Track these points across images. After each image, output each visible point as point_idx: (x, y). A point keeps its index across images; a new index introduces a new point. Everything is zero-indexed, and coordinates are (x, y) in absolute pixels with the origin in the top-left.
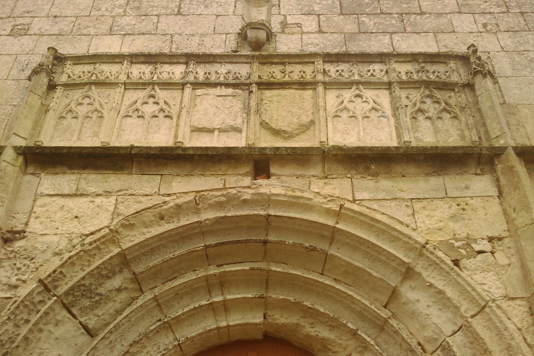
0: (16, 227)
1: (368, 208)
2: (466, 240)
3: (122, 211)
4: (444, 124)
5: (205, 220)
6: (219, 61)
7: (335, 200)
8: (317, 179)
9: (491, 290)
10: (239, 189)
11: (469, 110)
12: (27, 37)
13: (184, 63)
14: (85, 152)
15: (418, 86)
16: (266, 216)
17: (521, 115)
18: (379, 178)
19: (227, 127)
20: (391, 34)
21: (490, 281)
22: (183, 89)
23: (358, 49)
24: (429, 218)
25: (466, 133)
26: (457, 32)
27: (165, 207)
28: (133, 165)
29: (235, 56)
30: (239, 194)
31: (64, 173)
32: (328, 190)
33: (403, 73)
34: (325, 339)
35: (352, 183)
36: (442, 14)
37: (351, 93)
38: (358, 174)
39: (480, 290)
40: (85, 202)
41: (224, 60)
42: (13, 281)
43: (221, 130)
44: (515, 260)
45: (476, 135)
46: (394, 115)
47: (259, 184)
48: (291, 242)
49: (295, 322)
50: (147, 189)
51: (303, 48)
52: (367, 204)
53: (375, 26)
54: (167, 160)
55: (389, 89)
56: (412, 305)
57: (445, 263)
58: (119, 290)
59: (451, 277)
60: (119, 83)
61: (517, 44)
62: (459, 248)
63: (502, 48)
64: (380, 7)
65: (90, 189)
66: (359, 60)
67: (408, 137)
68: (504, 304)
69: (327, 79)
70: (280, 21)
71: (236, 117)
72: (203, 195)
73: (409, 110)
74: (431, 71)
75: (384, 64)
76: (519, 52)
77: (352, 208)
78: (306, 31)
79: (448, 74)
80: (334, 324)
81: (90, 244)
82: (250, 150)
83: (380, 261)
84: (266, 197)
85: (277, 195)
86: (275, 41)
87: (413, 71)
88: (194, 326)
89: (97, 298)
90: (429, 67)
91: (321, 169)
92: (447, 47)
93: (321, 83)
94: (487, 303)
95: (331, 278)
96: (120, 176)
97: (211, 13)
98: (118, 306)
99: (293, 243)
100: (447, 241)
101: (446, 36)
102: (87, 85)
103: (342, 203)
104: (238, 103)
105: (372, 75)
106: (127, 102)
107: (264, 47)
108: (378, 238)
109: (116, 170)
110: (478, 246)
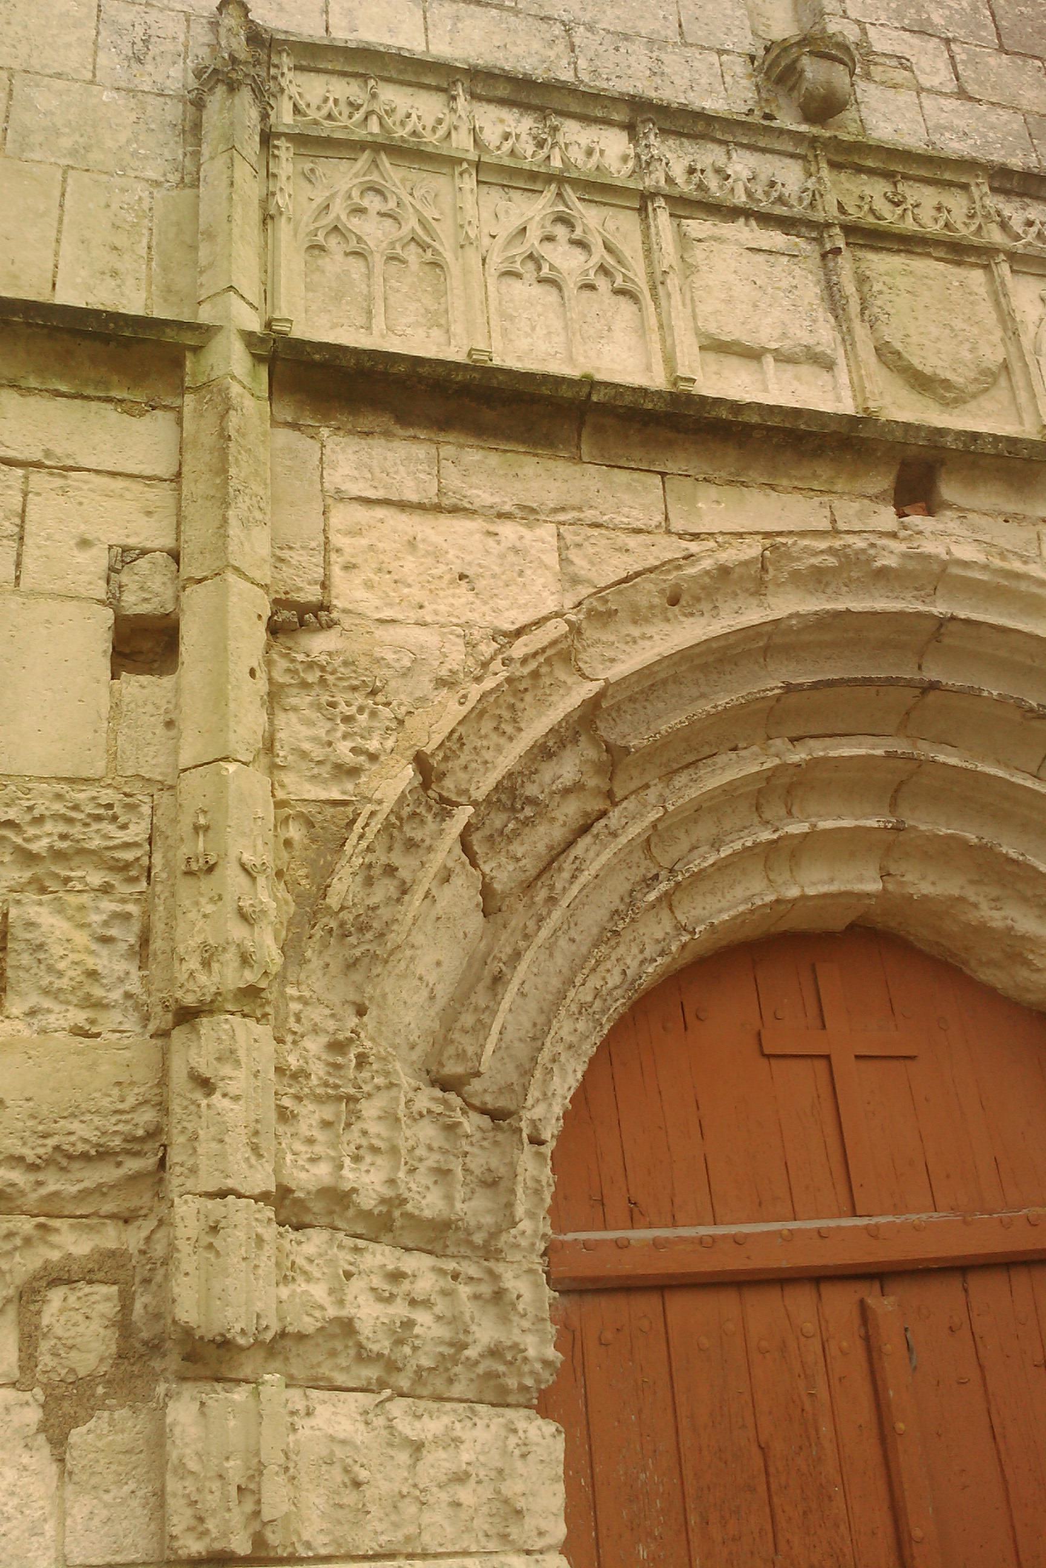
0: (299, 589)
3: (583, 572)
5: (791, 616)
6: (719, 135)
10: (873, 539)
14: (460, 378)
19: (797, 350)
22: (642, 210)
28: (580, 436)
30: (872, 552)
31: (387, 434)
34: (1030, 939)
40: (471, 534)
41: (735, 137)
42: (343, 749)
47: (916, 529)
48: (995, 693)
49: (956, 892)
54: (679, 432)
58: (567, 791)
60: (465, 160)
65: (479, 496)
71: (814, 321)
72: (785, 544)
81: (524, 661)
84: (935, 567)
85: (965, 564)
88: (719, 894)
96: (551, 464)
109: (535, 444)
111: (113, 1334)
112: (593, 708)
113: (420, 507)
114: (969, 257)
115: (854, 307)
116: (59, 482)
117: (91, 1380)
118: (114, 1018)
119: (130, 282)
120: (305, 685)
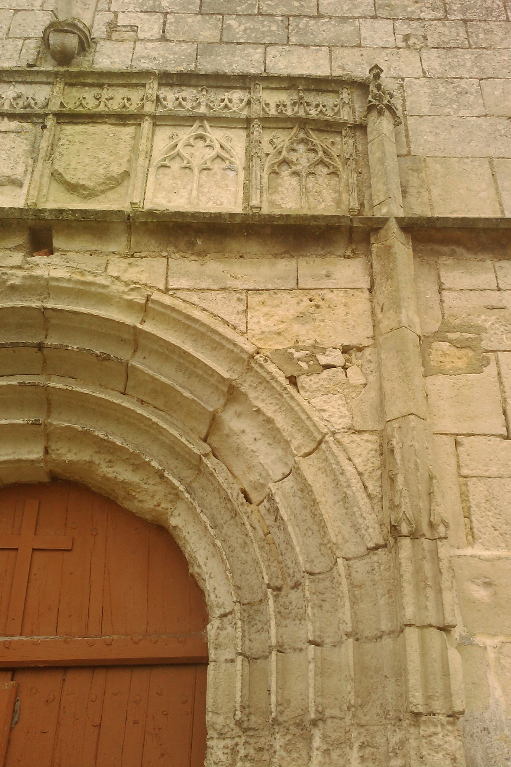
1: (184, 301)
2: (312, 349)
4: (316, 183)
7: (140, 288)
8: (118, 258)
9: (333, 420)
11: (354, 163)
15: (289, 125)
16: (40, 309)
17: (429, 173)
18: (207, 258)
20: (267, 45)
21: (333, 407)
22: (248, 128)
23: (213, 68)
24: (267, 317)
25: (344, 196)
26: (363, 47)
29: (30, 73)
30: (5, 277)
32: (132, 274)
33: (273, 106)
34: (126, 483)
35: (168, 264)
36: (348, 18)
37: (191, 133)
38: (178, 252)
39: (316, 419)
44: (375, 378)
45: (357, 200)
46: (248, 169)
47: (35, 263)
48: (75, 347)
49: (88, 458)
51: (133, 63)
53: (245, 34)
55: (248, 128)
56: (236, 437)
57: (277, 381)
59: (283, 400)
61: (447, 68)
62: (299, 360)
63: (424, 72)
64: (259, 4)
66: (212, 83)
67: (259, 200)
68: (346, 439)
69: (160, 110)
70: (107, 21)
71: (16, 163)
73: (268, 162)
74: (314, 104)
75: (247, 91)
76: (447, 81)
77: (161, 300)
78: (143, 37)
79: (336, 109)
80: (137, 463)
82: (21, 213)
83: (197, 376)
84: (42, 282)
86: (95, 51)
87: (288, 103)
90: (311, 98)
91: (126, 243)
92: (344, 69)
93: (149, 116)
94: (324, 437)
95: (136, 399)
97: (7, 7)
99: (78, 348)
100: (286, 350)
101: (346, 51)
102: (195, 121)
103: (149, 293)
104: (22, 142)
105: (226, 106)
107: (74, 60)
108: (197, 344)
110: (326, 358)
114: (130, 121)
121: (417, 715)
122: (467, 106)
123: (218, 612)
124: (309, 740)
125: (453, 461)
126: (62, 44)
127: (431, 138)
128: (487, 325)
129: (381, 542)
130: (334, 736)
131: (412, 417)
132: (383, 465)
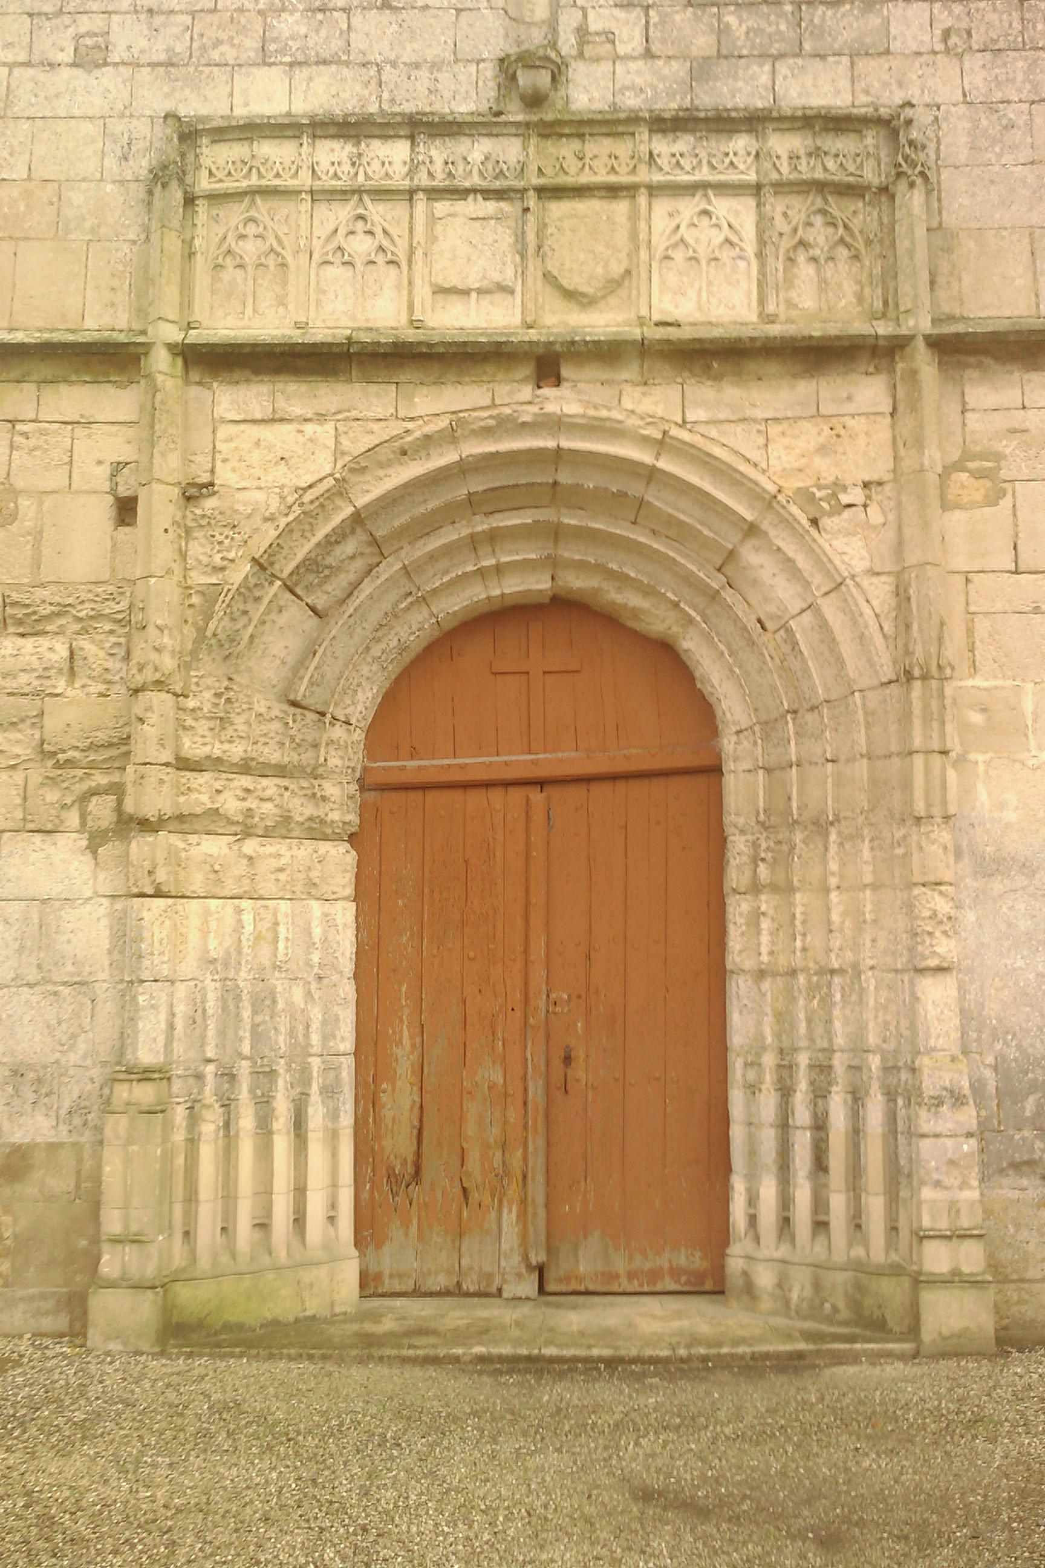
9: (853, 563)
12: (110, 69)
13: (406, 137)
15: (804, 188)
22: (411, 199)
25: (867, 291)
27: (409, 439)
31: (248, 381)
39: (837, 563)
42: (217, 559)
43: (480, 291)
46: (760, 255)
49: (596, 585)
50: (379, 409)
52: (702, 429)
58: (352, 558)
63: (965, 95)
73: (786, 243)
76: (991, 107)
79: (859, 160)
81: (312, 502)
87: (802, 153)
89: (327, 572)
98: (352, 577)
100: (807, 489)
101: (873, 63)
106: (321, 231)
111: (115, 814)
112: (357, 519)
113: (263, 421)
115: (531, 249)
116: (88, 431)
117: (107, 830)
118: (116, 688)
119: (121, 308)
120: (201, 526)
121: (918, 819)
122: (1013, 148)
123: (734, 729)
124: (826, 835)
125: (962, 599)
126: (534, 85)
127: (965, 200)
128: (1008, 451)
129: (894, 678)
130: (847, 832)
131: (928, 567)
132: (899, 607)
